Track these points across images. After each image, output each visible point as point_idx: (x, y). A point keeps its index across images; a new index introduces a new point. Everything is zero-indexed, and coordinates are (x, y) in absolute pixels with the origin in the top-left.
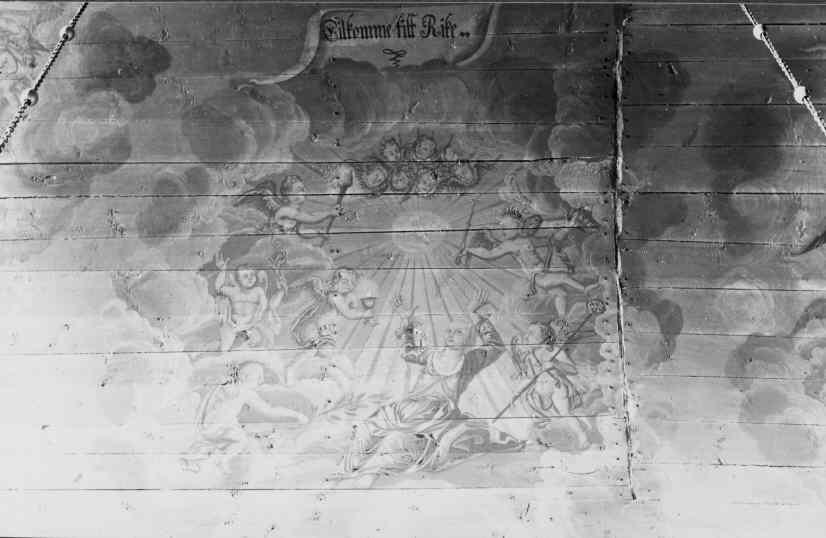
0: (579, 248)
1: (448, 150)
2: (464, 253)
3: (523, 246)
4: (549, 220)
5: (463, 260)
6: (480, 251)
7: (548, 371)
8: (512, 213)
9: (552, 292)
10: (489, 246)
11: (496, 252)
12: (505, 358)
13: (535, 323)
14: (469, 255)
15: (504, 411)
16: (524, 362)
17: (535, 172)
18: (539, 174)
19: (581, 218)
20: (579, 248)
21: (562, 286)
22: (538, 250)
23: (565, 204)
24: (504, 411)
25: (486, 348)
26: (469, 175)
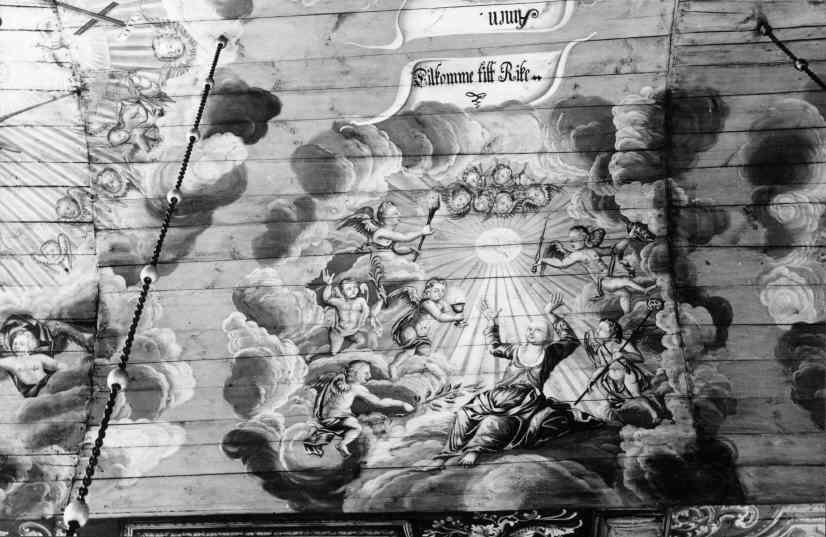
0: (639, 256)
1: (522, 176)
2: (539, 263)
3: (590, 255)
4: (613, 232)
5: (539, 269)
6: (556, 262)
7: (618, 360)
8: (577, 228)
9: (618, 293)
10: (561, 256)
11: (567, 261)
12: (581, 350)
13: (603, 320)
14: (544, 264)
15: (583, 395)
16: (597, 353)
17: (598, 193)
18: (603, 195)
19: (638, 230)
20: (639, 256)
21: (625, 288)
22: (603, 258)
23: (625, 219)
24: (583, 395)
25: (564, 343)
26: (541, 197)
